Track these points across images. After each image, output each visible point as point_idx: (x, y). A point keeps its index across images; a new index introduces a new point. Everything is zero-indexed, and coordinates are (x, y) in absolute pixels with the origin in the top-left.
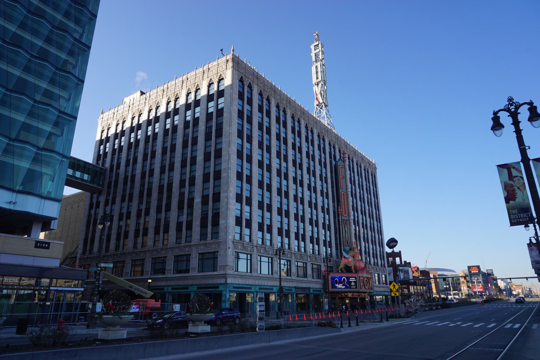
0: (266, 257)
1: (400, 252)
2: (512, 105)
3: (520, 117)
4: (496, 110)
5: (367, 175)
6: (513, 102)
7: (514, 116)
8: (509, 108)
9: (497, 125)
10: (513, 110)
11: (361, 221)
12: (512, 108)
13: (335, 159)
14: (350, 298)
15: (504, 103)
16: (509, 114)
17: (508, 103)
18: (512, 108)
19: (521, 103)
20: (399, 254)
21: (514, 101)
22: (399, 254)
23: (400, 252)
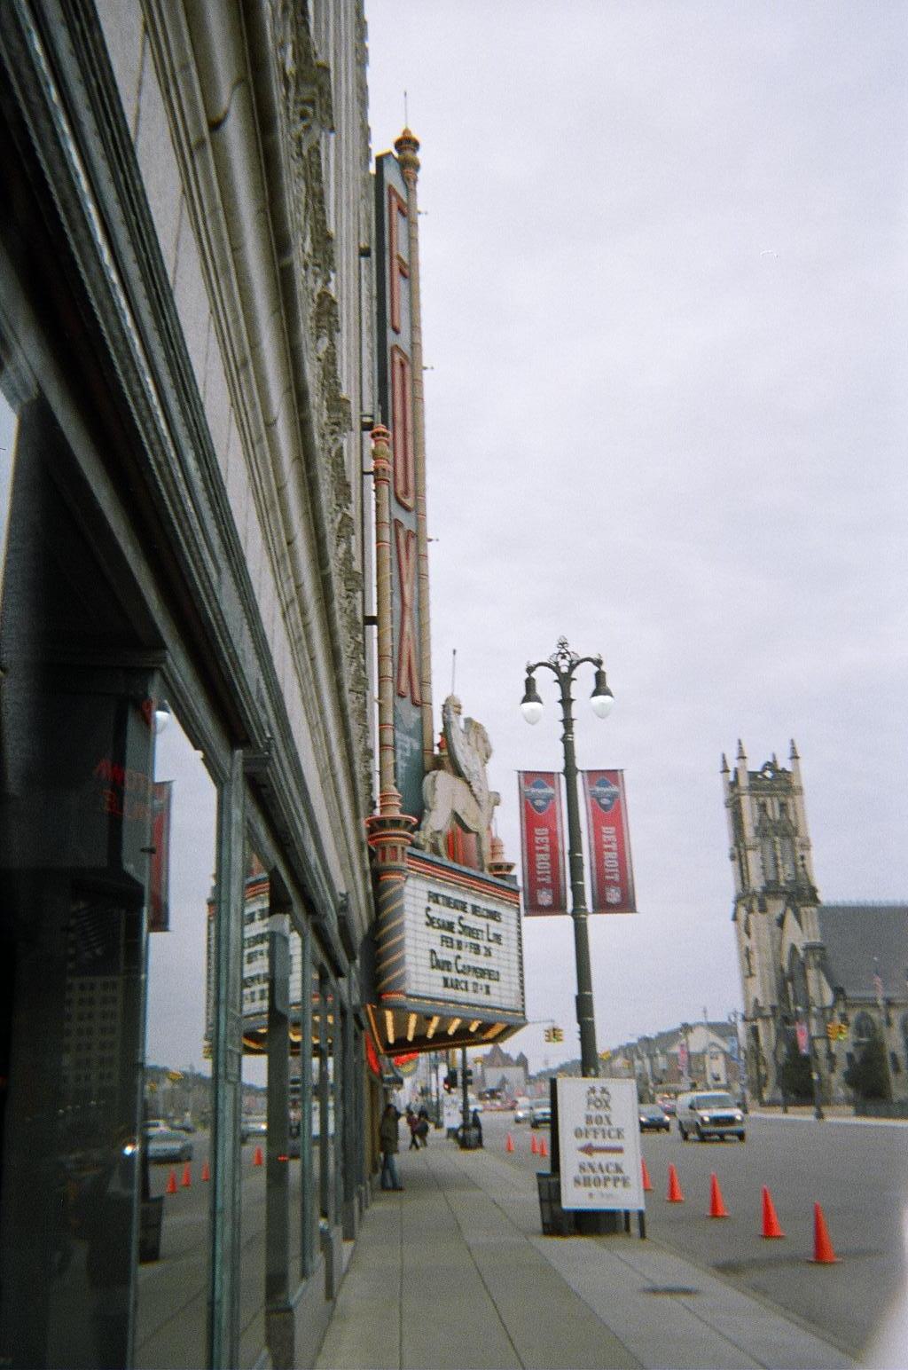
2: (564, 657)
6: (568, 653)
8: (557, 663)
9: (530, 694)
10: (564, 670)
15: (548, 652)
16: (557, 678)
17: (557, 651)
19: (582, 657)
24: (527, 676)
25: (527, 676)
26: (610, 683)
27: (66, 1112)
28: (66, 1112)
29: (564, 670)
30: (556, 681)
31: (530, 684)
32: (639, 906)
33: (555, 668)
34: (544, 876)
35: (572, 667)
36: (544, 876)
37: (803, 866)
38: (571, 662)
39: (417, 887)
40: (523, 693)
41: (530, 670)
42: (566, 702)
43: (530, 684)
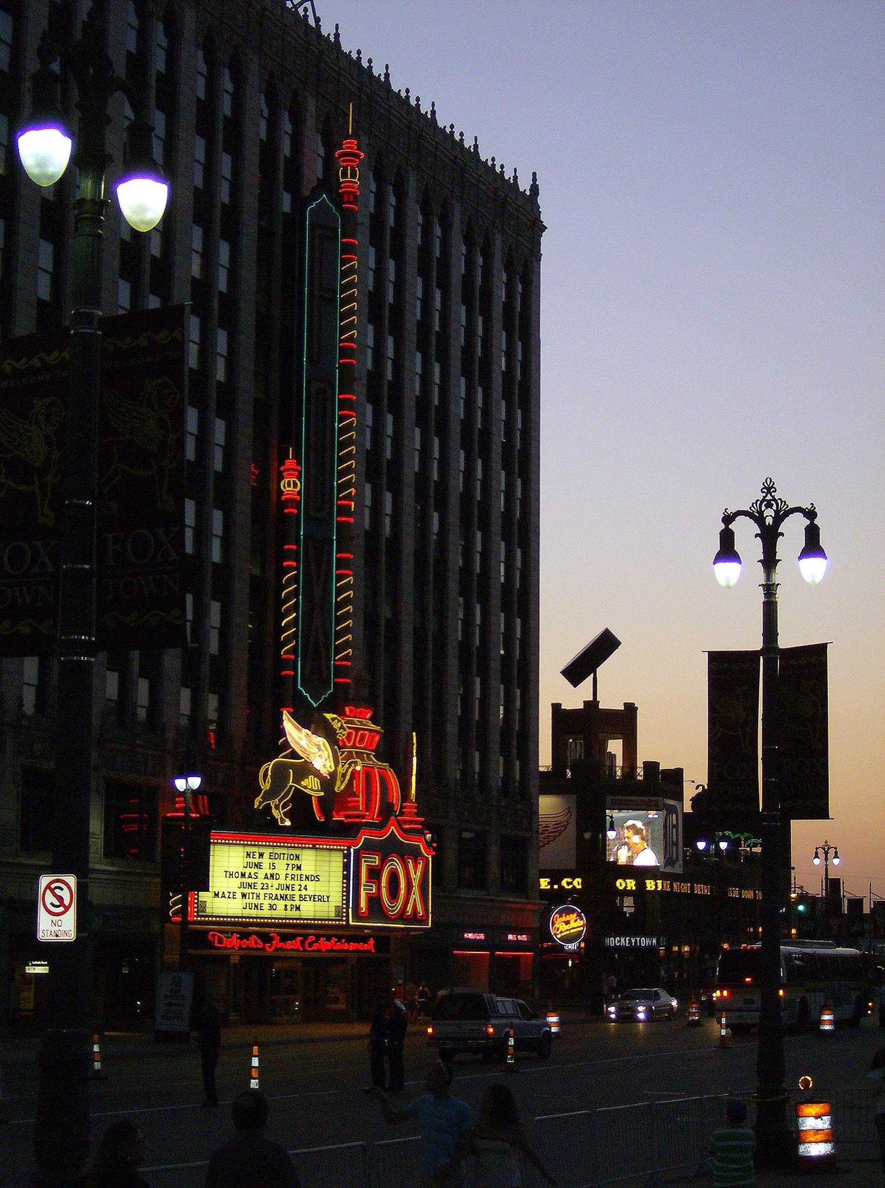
0: (340, 850)
1: (631, 709)
2: (769, 505)
3: (781, 544)
4: (732, 510)
5: (475, 238)
6: (774, 499)
7: (769, 536)
8: (761, 513)
9: (727, 550)
11: (458, 340)
12: (769, 514)
13: (294, 183)
14: (777, 809)
15: (748, 496)
17: (760, 496)
18: (769, 514)
20: (625, 721)
21: (777, 495)
22: (625, 721)
23: (631, 709)
24: (723, 526)
25: (723, 526)
26: (824, 541)
27: (711, 1010)
28: (711, 1010)
29: (769, 521)
30: (757, 535)
31: (817, 853)
32: (602, 629)
33: (759, 519)
34: (656, 885)
35: (779, 518)
36: (656, 885)
37: (284, 938)
38: (777, 512)
39: (332, 884)
40: (717, 548)
41: (728, 519)
42: (770, 562)
43: (817, 853)
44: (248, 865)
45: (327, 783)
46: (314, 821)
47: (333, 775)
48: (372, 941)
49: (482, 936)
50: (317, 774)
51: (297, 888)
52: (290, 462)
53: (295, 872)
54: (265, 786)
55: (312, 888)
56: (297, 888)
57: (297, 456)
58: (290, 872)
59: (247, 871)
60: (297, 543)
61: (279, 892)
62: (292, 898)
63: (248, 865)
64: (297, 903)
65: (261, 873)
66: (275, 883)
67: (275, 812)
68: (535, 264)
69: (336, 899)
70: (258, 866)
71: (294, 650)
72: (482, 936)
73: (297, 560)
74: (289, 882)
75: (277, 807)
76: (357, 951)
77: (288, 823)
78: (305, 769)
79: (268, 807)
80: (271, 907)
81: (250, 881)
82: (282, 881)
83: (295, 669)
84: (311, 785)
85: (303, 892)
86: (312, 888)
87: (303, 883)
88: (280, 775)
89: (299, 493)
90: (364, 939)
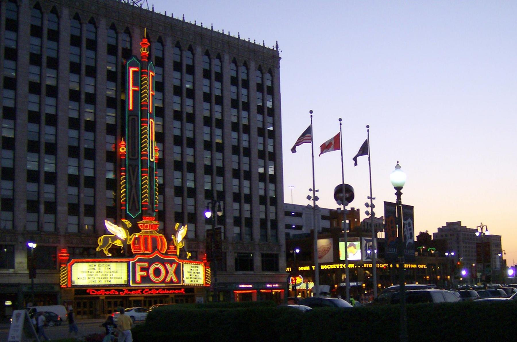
44: (90, 269)
45: (124, 242)
46: (120, 253)
47: (126, 239)
48: (183, 290)
49: (240, 286)
50: (120, 239)
51: (109, 275)
52: (123, 143)
53: (109, 270)
54: (100, 244)
55: (115, 275)
56: (109, 275)
57: (125, 140)
58: (106, 270)
59: (90, 271)
60: (125, 167)
61: (102, 277)
62: (108, 278)
63: (90, 269)
64: (109, 280)
65: (95, 271)
66: (100, 274)
67: (105, 252)
68: (276, 69)
69: (125, 278)
70: (94, 269)
71: (125, 200)
72: (240, 286)
73: (125, 172)
74: (106, 273)
75: (106, 250)
76: (174, 293)
77: (110, 255)
78: (115, 238)
79: (102, 250)
80: (100, 281)
81: (91, 274)
82: (103, 273)
83: (126, 207)
84: (118, 243)
85: (112, 276)
86: (115, 275)
87: (112, 274)
88: (106, 240)
89: (126, 152)
90: (180, 289)
